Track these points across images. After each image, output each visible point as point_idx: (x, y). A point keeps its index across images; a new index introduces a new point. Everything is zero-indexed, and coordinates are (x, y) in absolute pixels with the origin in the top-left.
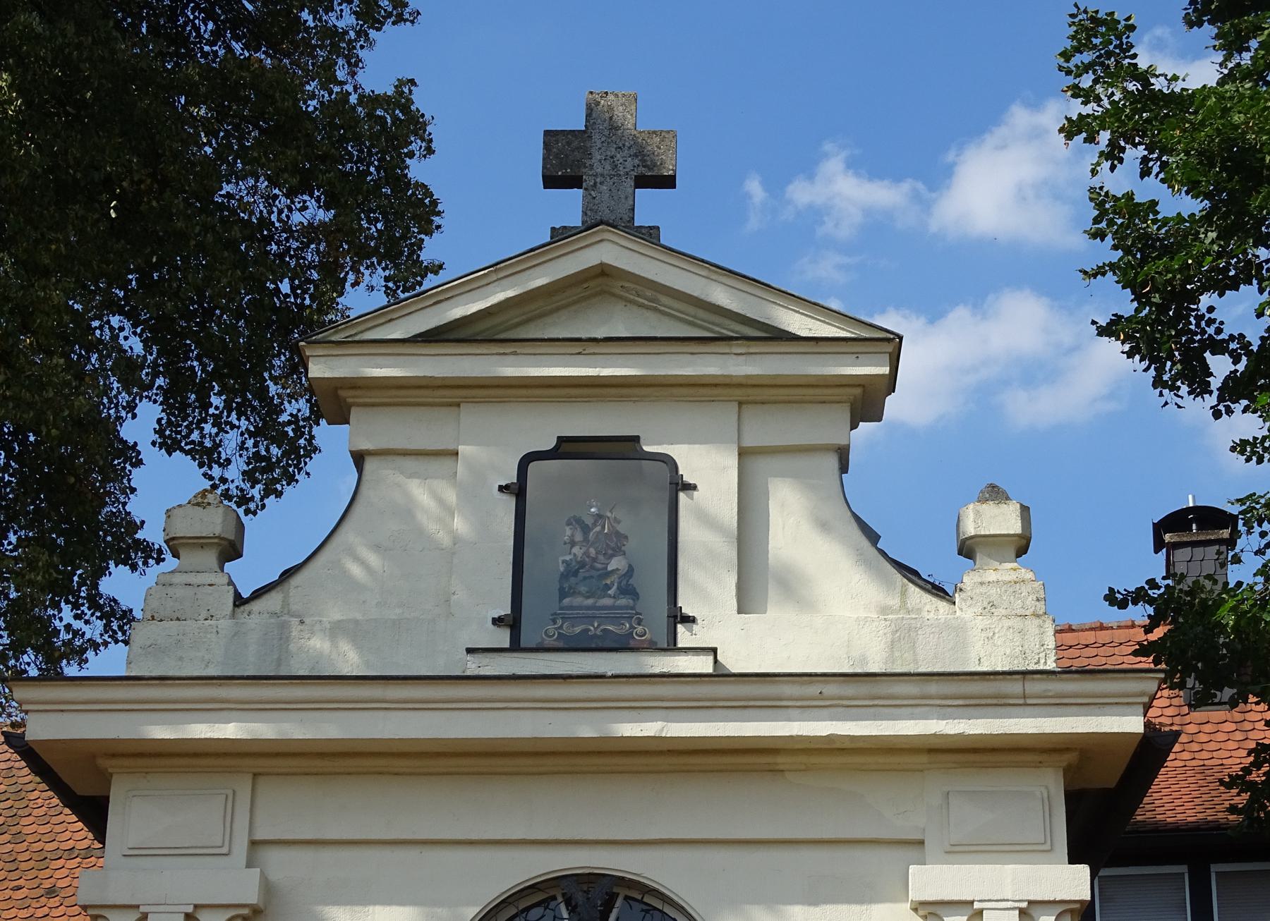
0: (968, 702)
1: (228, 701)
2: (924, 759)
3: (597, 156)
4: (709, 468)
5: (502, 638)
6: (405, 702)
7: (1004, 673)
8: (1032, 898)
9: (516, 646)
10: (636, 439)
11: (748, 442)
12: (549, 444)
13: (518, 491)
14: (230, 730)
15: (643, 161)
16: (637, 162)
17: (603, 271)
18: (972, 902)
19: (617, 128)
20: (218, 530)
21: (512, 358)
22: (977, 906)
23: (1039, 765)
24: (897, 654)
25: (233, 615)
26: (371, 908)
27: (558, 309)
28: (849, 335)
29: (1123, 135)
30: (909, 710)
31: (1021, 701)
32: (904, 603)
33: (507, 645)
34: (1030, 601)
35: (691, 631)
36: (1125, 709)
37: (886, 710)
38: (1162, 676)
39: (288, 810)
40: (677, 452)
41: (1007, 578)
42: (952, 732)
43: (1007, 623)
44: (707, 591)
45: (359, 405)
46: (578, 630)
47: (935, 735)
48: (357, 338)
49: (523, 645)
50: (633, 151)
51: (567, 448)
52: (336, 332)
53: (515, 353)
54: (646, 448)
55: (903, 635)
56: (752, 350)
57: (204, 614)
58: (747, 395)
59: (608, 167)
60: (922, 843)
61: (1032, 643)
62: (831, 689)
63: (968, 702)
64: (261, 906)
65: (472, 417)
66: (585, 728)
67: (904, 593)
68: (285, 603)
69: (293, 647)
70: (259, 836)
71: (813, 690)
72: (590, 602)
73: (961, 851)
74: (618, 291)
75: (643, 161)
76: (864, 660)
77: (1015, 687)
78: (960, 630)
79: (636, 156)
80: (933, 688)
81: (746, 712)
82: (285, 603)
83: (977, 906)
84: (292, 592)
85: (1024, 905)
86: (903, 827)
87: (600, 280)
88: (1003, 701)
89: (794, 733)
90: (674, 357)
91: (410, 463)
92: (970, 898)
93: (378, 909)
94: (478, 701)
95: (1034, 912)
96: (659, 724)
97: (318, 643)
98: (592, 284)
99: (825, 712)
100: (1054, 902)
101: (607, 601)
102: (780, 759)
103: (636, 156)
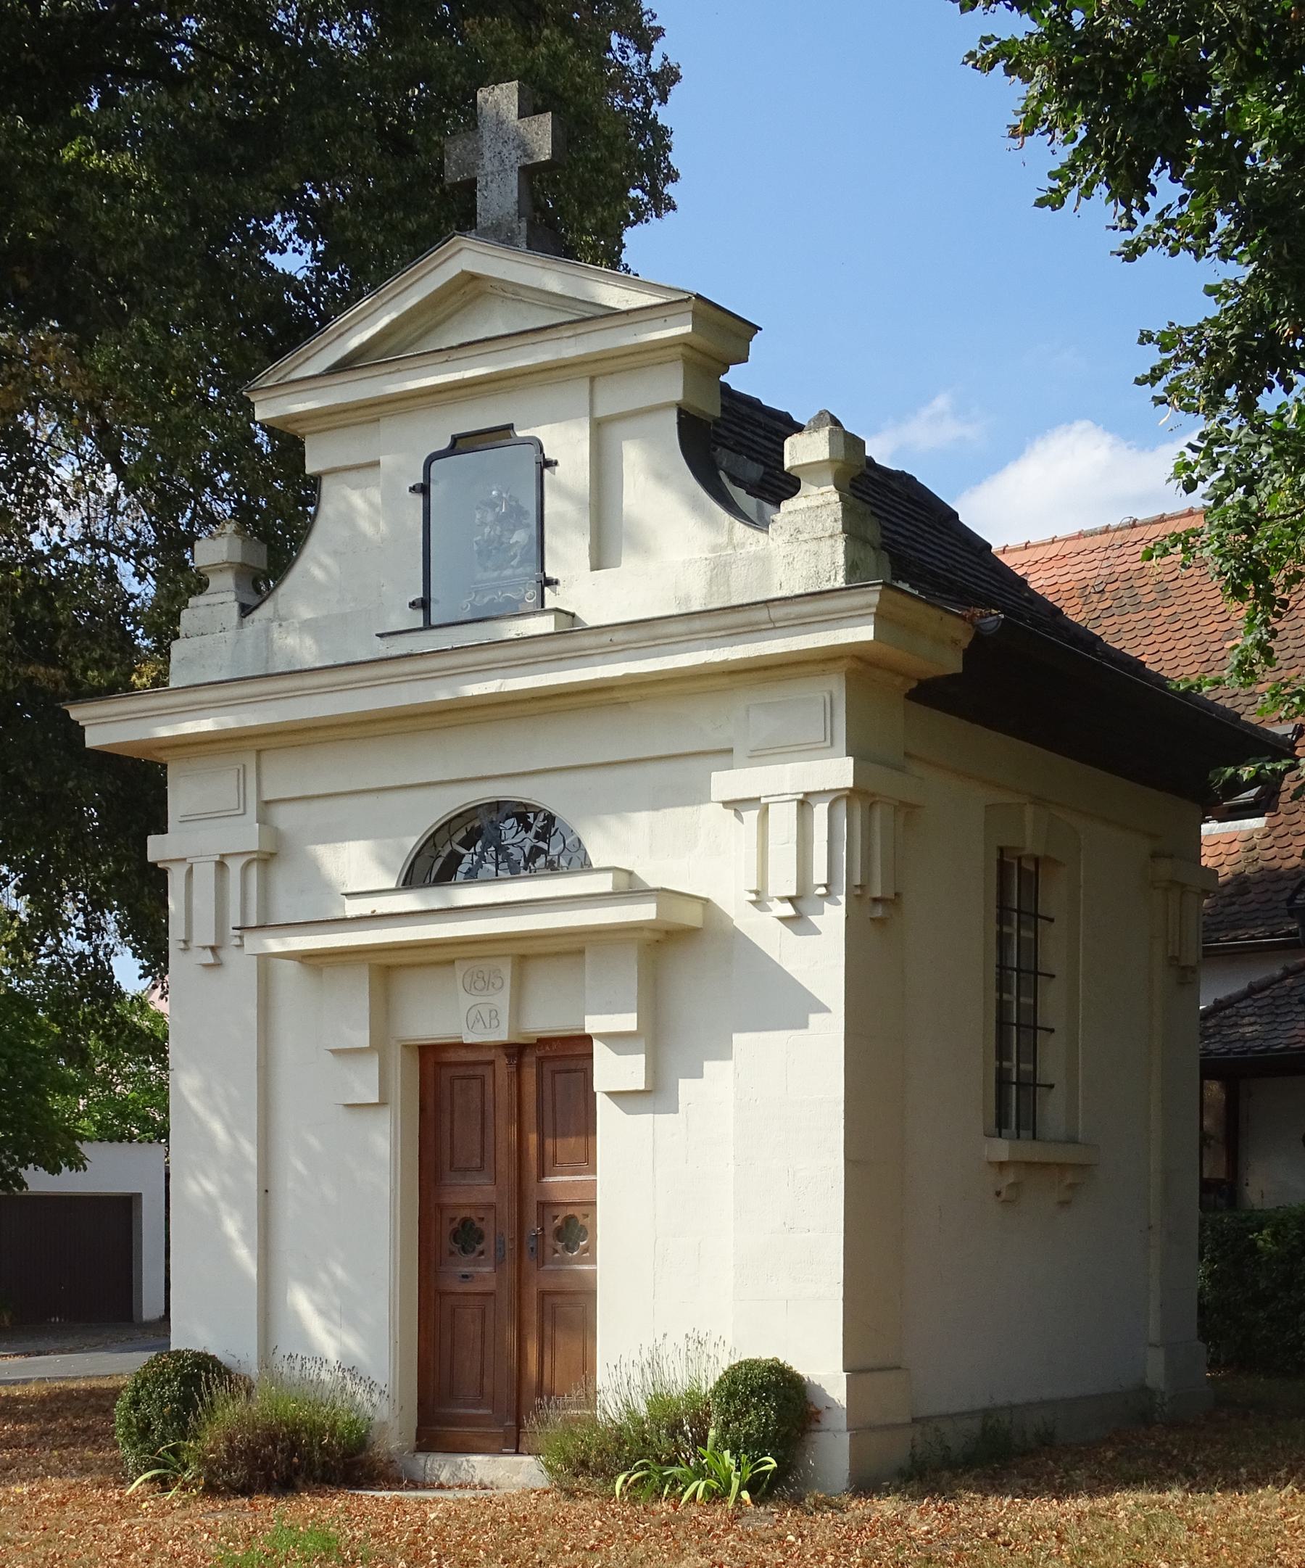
0: (729, 632)
1: (351, 683)
2: (725, 681)
3: (488, 155)
4: (566, 443)
5: (417, 618)
6: (351, 683)
7: (748, 605)
8: (806, 790)
9: (428, 625)
10: (510, 427)
11: (600, 413)
12: (445, 444)
13: (423, 489)
14: (206, 725)
15: (524, 150)
16: (519, 152)
17: (470, 278)
18: (759, 799)
19: (502, 123)
20: (225, 557)
21: (398, 375)
22: (763, 801)
23: (823, 672)
24: (714, 589)
25: (241, 625)
26: (347, 844)
27: (449, 316)
28: (576, 318)
29: (273, 278)
30: (685, 645)
31: (771, 626)
32: (731, 539)
33: (421, 625)
34: (829, 523)
35: (554, 591)
36: (835, 624)
37: (667, 647)
38: (880, 588)
39: (284, 777)
40: (543, 433)
41: (815, 503)
42: (718, 660)
43: (805, 547)
44: (567, 552)
45: (310, 433)
46: (486, 600)
47: (705, 664)
48: (287, 379)
49: (433, 622)
50: (517, 142)
51: (460, 444)
52: (269, 377)
53: (399, 371)
54: (519, 434)
55: (719, 570)
56: (579, 331)
57: (220, 628)
58: (594, 370)
59: (497, 164)
60: (730, 751)
61: (825, 564)
62: (619, 636)
63: (729, 632)
64: (269, 849)
65: (390, 430)
66: (442, 693)
67: (731, 531)
68: (276, 611)
69: (275, 647)
70: (266, 798)
71: (605, 639)
72: (496, 574)
73: (760, 755)
74: (490, 290)
75: (524, 150)
76: (688, 599)
77: (761, 615)
78: (763, 561)
79: (519, 147)
80: (697, 624)
81: (562, 663)
82: (276, 611)
83: (763, 801)
84: (280, 600)
85: (800, 797)
86: (716, 740)
87: (471, 286)
88: (756, 628)
89: (598, 676)
90: (520, 349)
91: (353, 476)
92: (757, 795)
93: (351, 843)
94: (369, 680)
95: (811, 800)
96: (498, 682)
97: (291, 641)
98: (467, 289)
99: (621, 655)
100: (825, 792)
101: (508, 572)
102: (616, 694)
103: (519, 147)
